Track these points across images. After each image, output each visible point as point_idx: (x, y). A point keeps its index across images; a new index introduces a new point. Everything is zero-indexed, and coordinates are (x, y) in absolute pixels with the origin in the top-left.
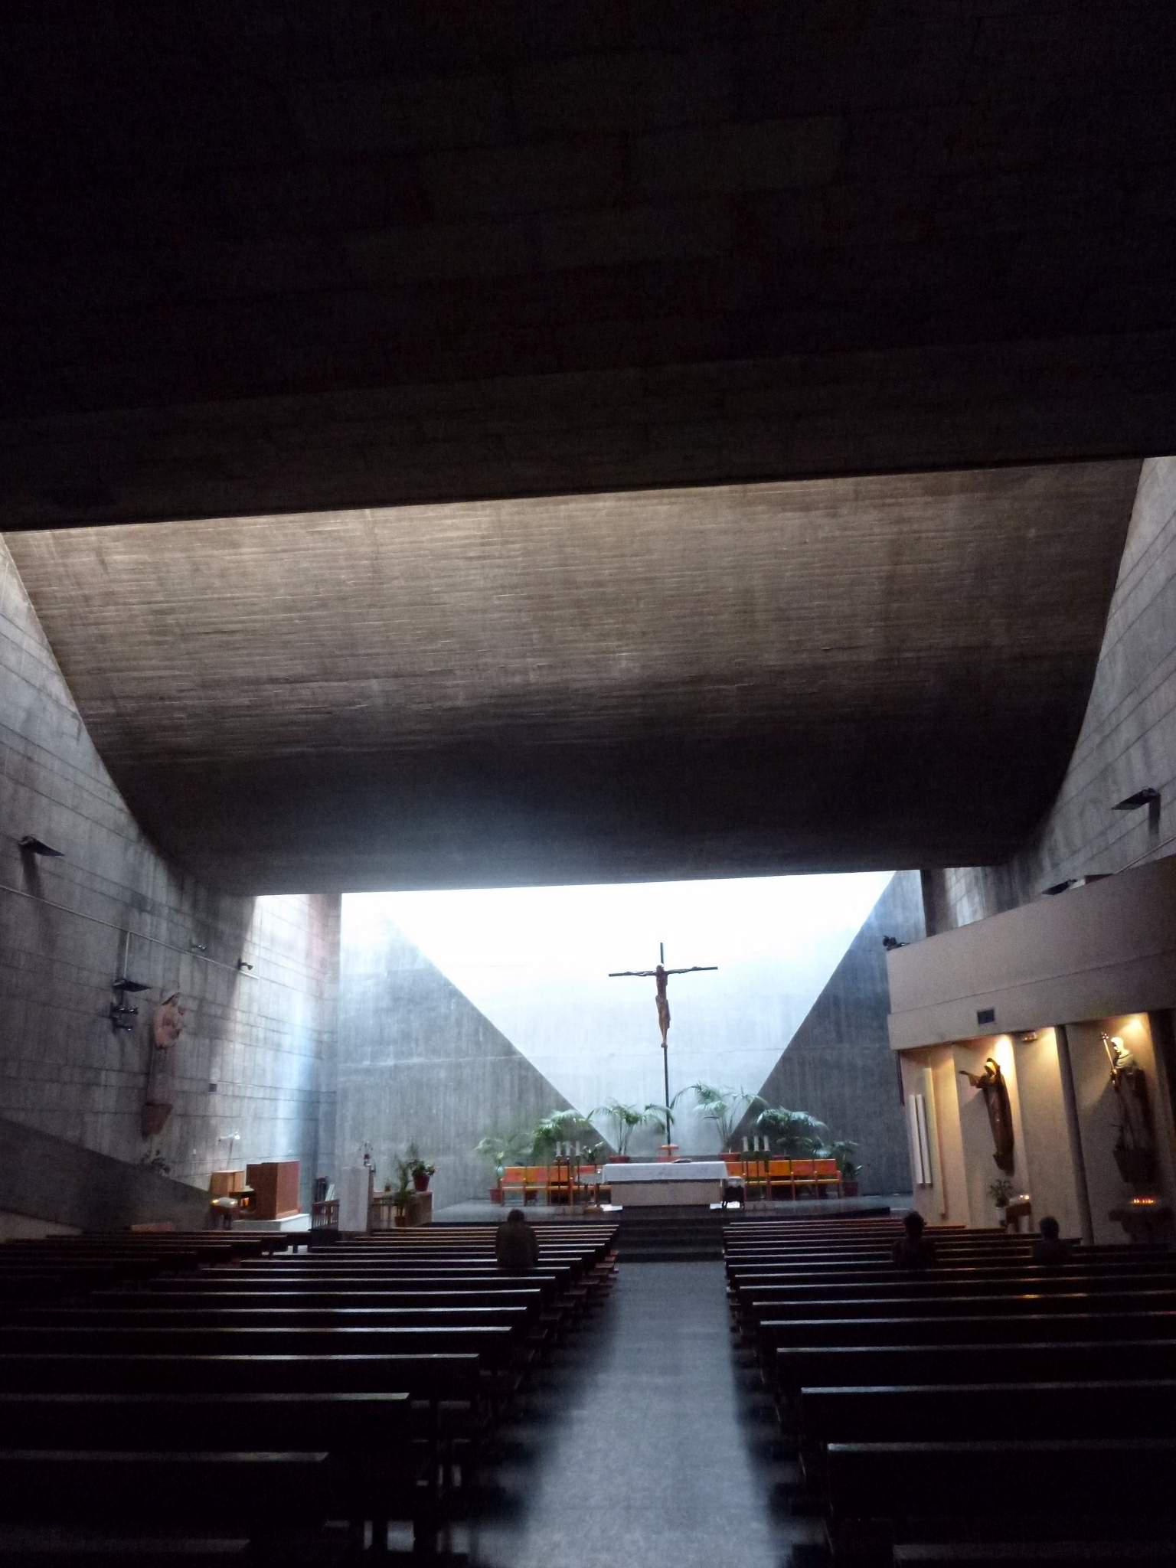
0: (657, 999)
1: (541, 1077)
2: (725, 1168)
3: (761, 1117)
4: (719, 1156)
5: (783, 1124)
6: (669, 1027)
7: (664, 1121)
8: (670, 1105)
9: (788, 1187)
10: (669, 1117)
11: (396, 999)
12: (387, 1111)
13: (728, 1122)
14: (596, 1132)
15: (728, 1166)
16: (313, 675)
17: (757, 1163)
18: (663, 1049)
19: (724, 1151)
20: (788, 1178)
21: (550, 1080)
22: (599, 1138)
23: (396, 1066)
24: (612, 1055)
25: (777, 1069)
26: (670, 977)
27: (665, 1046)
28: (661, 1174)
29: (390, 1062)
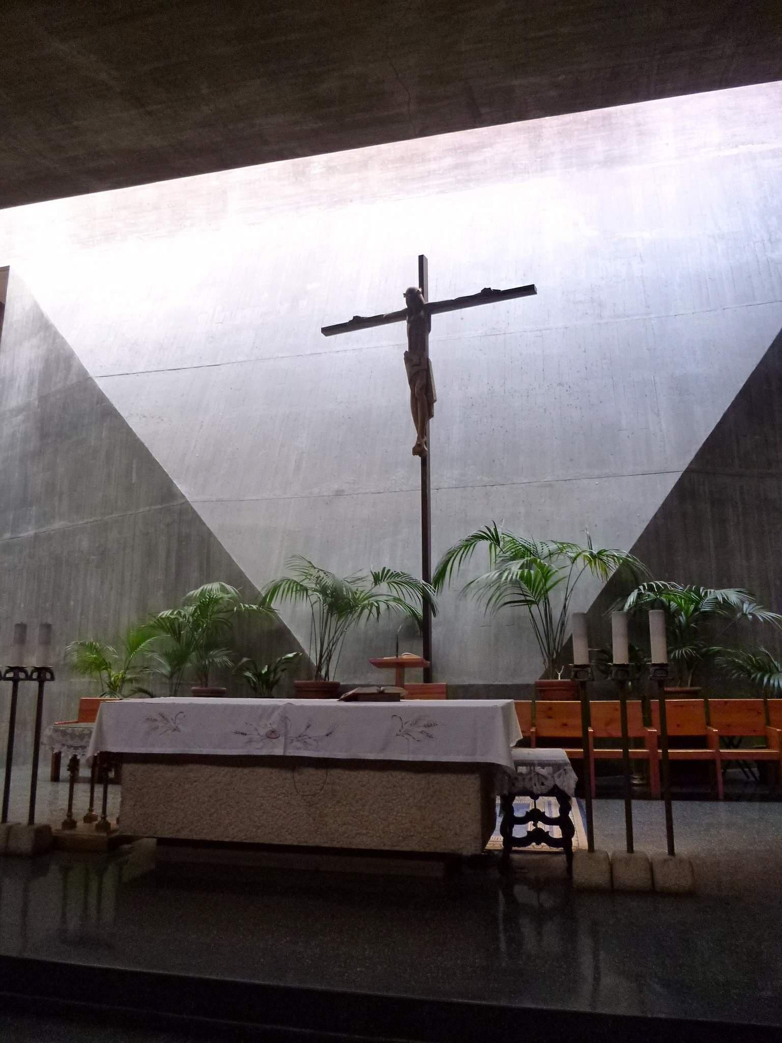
0: (408, 357)
1: (210, 533)
2: (514, 706)
3: (632, 598)
4: (538, 685)
5: (683, 619)
6: (431, 415)
7: (420, 611)
8: (433, 572)
9: (703, 767)
10: (428, 604)
11: (44, 436)
12: (22, 606)
13: (556, 614)
14: (289, 632)
15: (516, 704)
16: (467, 589)
17: (624, 707)
18: (418, 459)
19: (546, 676)
20: (700, 741)
21: (227, 544)
22: (292, 643)
23: (36, 536)
24: (339, 493)
25: (666, 511)
26: (436, 319)
27: (421, 450)
28: (272, 735)
29: (31, 532)
